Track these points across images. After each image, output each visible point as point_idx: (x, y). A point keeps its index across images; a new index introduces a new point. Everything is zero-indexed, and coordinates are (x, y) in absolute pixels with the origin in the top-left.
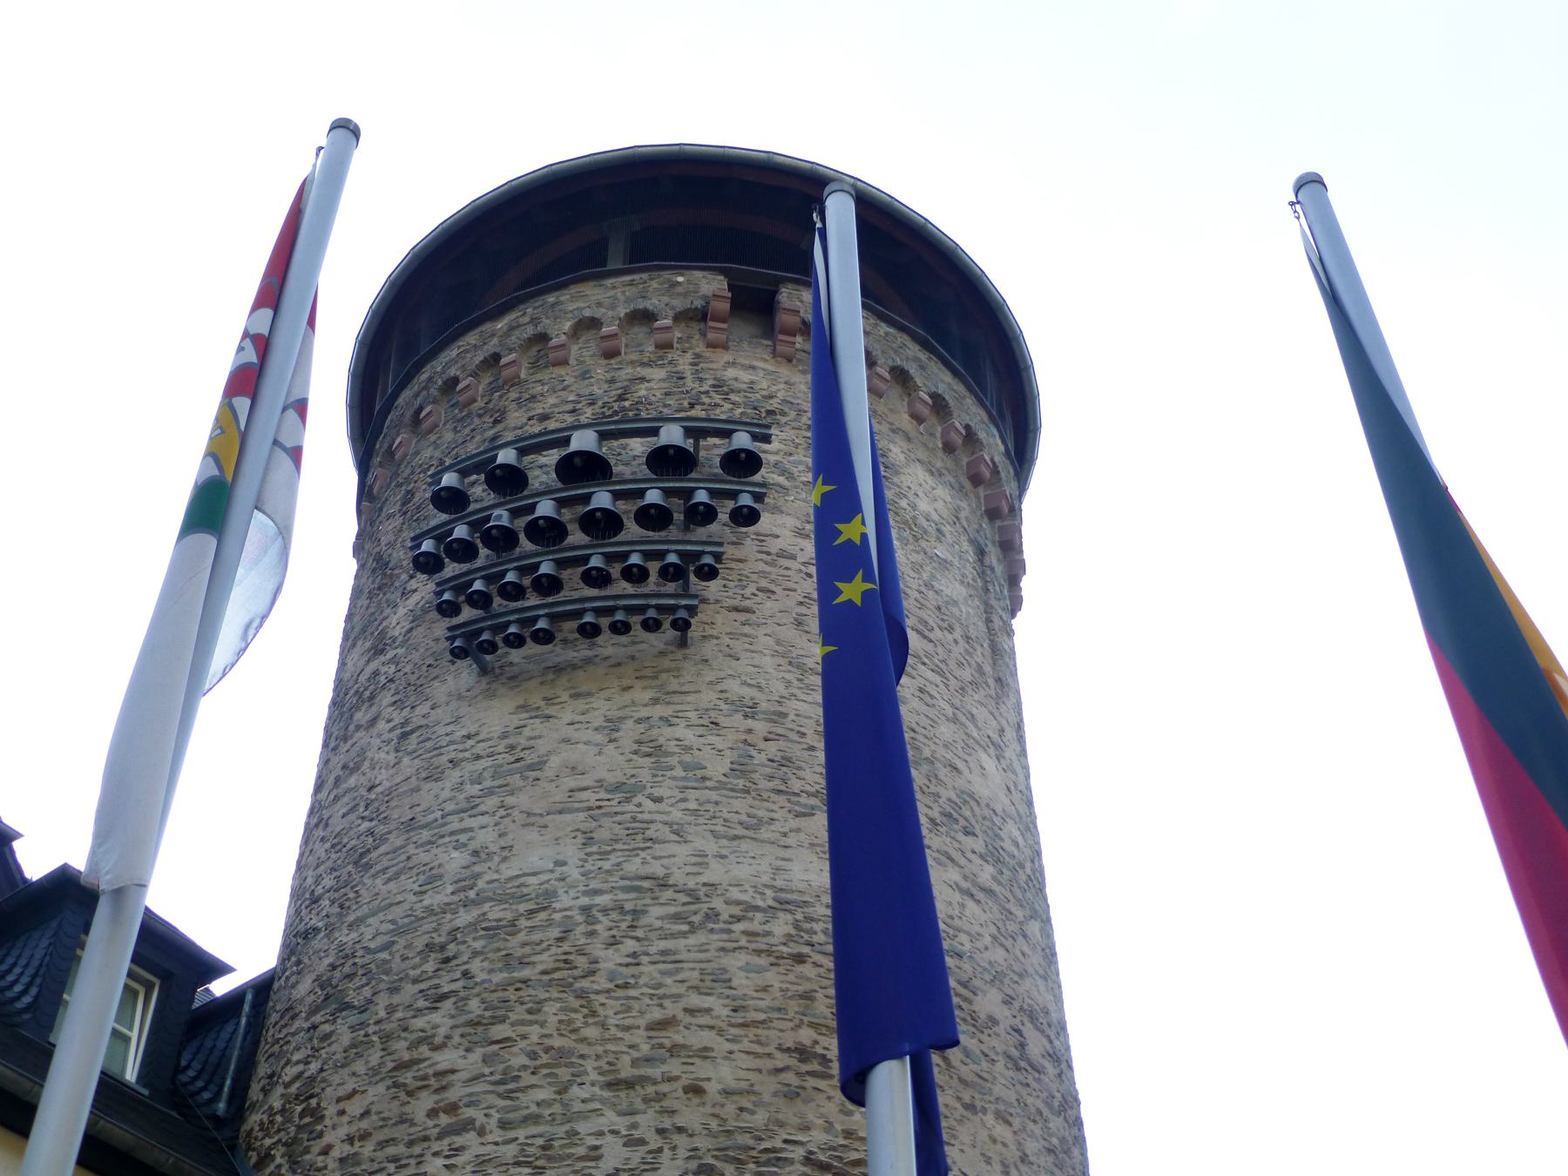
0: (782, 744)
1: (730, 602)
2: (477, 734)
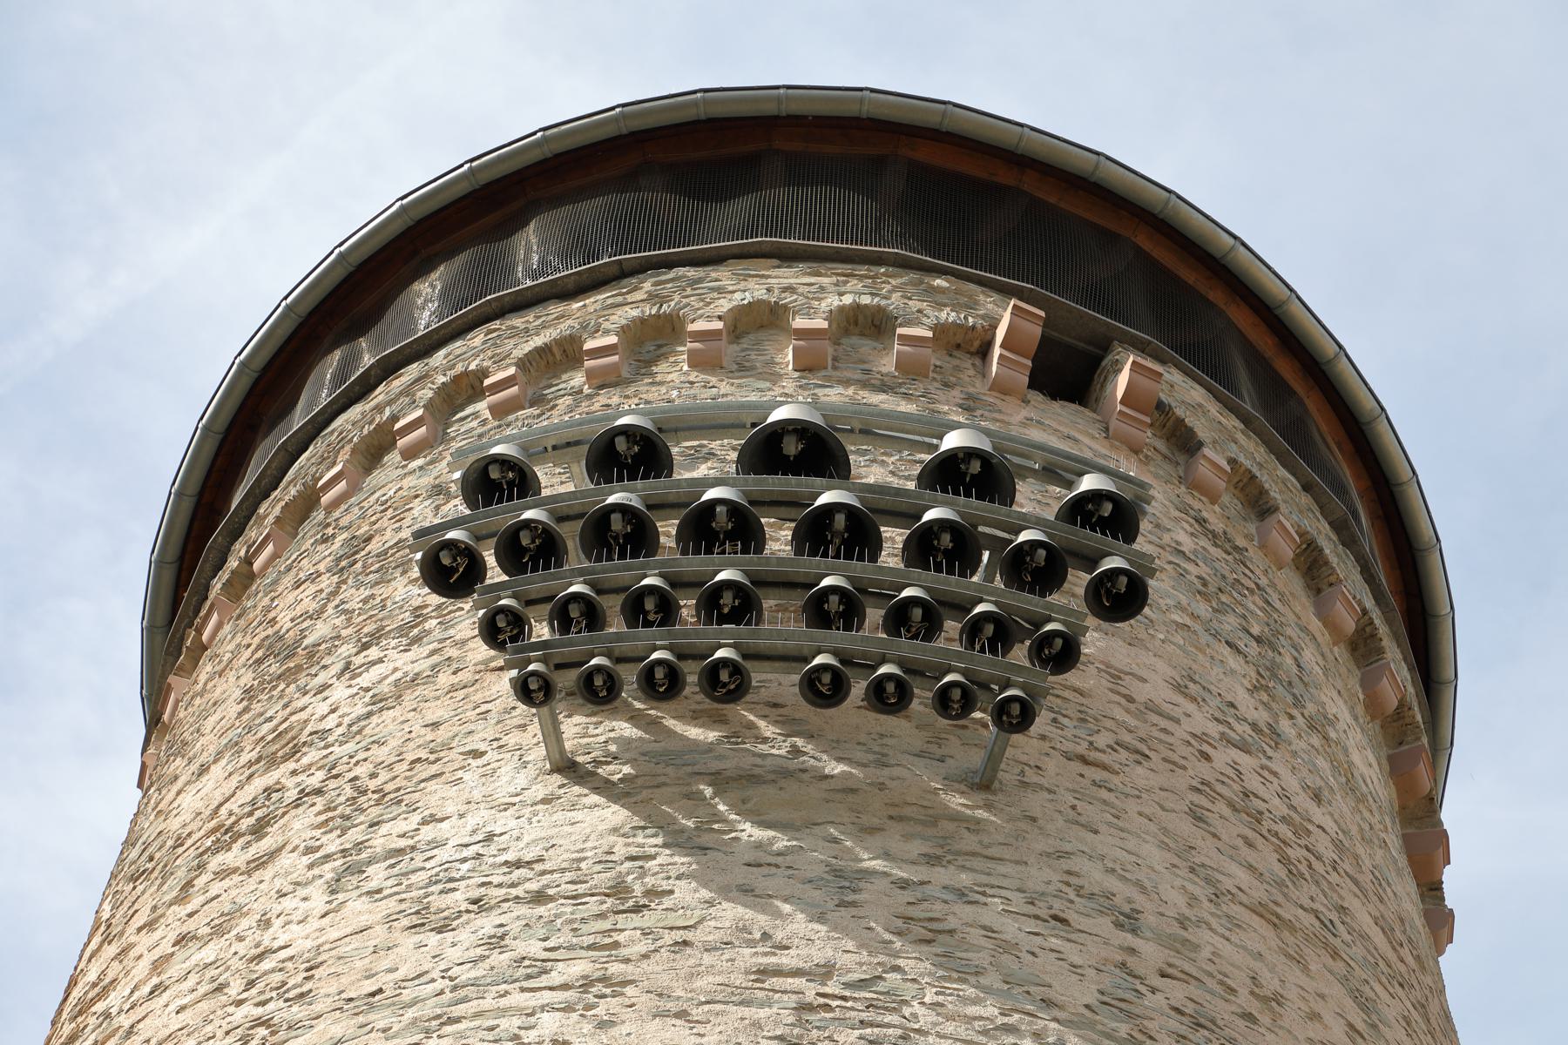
0: (1193, 990)
1: (1068, 746)
2: (540, 860)
